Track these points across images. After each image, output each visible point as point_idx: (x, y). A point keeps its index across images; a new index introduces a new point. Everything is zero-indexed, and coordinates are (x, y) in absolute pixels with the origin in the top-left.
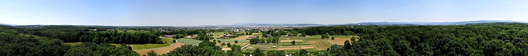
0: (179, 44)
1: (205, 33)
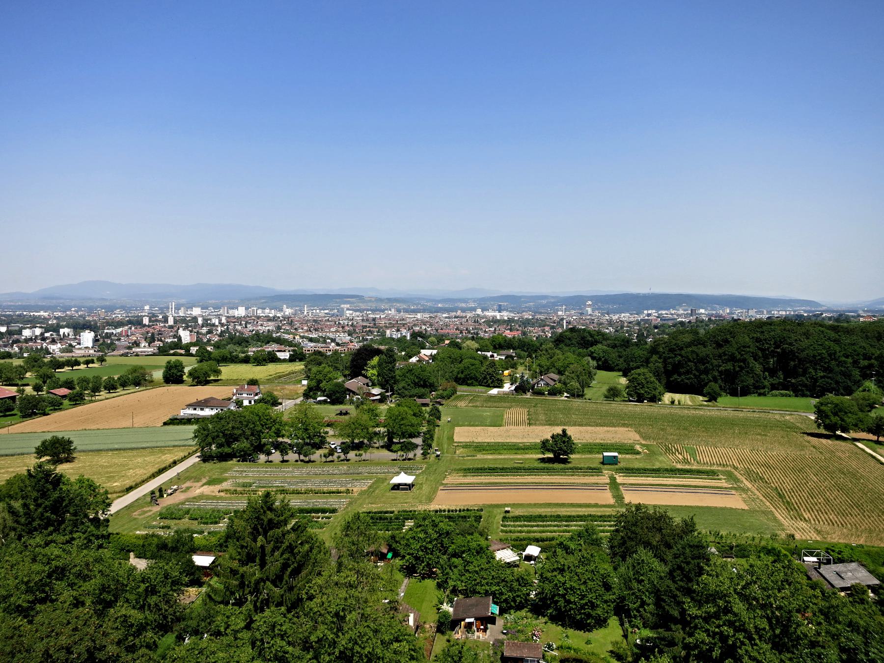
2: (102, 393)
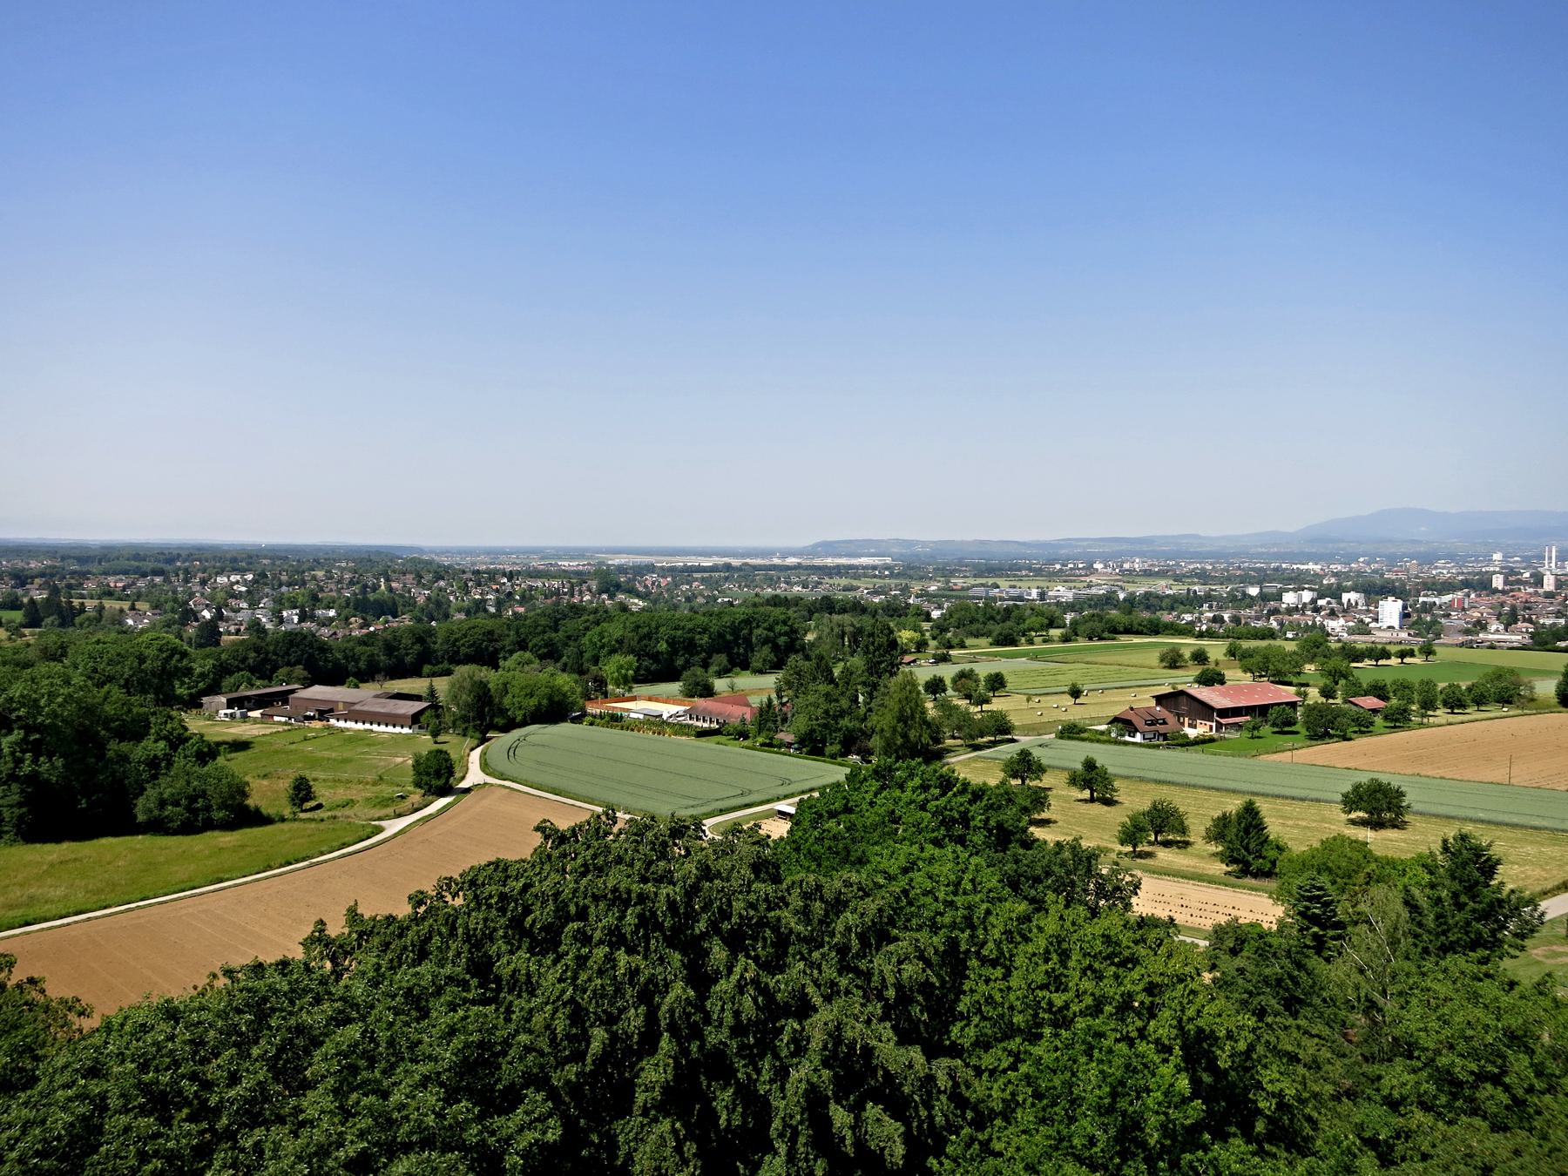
0: (511, 804)
1: (885, 655)
2: (1438, 712)
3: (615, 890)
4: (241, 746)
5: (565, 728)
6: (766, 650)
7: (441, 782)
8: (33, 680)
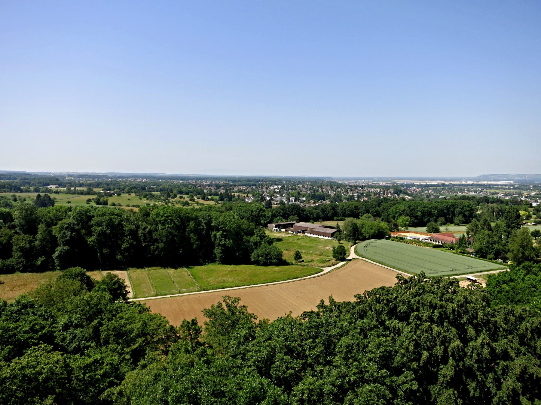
0: (368, 270)
1: (515, 221)
3: (431, 302)
4: (279, 240)
5: (383, 241)
6: (461, 216)
7: (342, 256)
8: (225, 217)
